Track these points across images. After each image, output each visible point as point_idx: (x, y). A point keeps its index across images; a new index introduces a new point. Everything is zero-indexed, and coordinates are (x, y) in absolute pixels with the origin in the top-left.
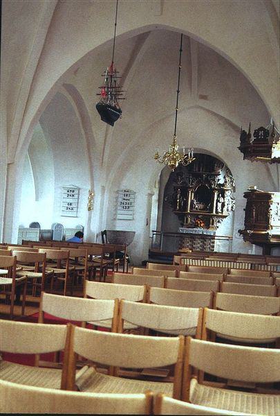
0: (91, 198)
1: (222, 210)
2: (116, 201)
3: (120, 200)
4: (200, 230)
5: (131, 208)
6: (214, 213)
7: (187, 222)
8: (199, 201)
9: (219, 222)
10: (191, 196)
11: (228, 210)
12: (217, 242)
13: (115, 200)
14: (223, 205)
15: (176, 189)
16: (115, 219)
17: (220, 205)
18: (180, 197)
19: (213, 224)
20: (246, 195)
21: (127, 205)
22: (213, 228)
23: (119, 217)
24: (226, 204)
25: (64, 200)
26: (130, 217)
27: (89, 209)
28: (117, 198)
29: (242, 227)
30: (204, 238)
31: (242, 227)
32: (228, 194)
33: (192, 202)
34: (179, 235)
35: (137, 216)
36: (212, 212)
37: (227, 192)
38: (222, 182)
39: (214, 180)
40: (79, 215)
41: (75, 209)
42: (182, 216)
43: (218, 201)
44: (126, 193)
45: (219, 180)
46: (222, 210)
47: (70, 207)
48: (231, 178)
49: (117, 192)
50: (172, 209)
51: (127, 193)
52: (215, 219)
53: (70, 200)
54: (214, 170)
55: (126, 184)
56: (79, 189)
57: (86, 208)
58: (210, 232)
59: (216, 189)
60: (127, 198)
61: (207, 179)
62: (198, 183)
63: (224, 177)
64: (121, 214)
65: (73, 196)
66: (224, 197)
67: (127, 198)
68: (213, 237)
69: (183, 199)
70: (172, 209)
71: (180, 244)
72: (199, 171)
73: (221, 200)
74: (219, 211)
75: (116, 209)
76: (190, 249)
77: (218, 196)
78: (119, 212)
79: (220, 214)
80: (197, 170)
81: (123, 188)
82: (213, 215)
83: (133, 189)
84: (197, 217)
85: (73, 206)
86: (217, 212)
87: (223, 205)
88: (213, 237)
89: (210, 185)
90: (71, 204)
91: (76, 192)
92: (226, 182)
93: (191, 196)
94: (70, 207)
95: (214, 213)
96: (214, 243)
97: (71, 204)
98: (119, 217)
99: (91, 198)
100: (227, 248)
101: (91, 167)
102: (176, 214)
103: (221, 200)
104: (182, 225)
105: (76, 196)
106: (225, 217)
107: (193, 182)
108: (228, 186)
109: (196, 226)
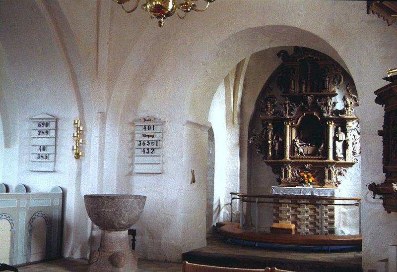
0: (80, 134)
1: (344, 154)
2: (133, 141)
3: (138, 137)
4: (308, 189)
5: (157, 152)
6: (331, 159)
7: (286, 177)
8: (305, 140)
9: (340, 174)
10: (291, 134)
11: (354, 153)
12: (338, 211)
13: (129, 138)
14: (345, 145)
15: (265, 125)
16: (130, 174)
17: (339, 145)
18: (272, 137)
19: (330, 178)
20: (377, 101)
21: (150, 146)
22: (330, 184)
23: (138, 168)
24: (350, 143)
25: (34, 142)
26: (156, 168)
27: (77, 156)
28: (133, 134)
29: (379, 178)
30: (314, 201)
31: (379, 178)
32: (352, 125)
33: (293, 143)
34: (272, 200)
35: (169, 166)
36: (327, 157)
37: (350, 123)
38: (340, 106)
39: (326, 105)
40: (60, 167)
41: (51, 157)
42: (278, 167)
43: (336, 139)
44: (147, 124)
45: (335, 104)
46: (344, 154)
47: (43, 154)
48: (355, 99)
49: (133, 124)
50: (262, 156)
51: (150, 124)
52: (334, 170)
53: (43, 141)
54: (324, 88)
55: (146, 108)
56: (57, 120)
57: (71, 155)
58: (325, 191)
59: (331, 119)
60: (150, 132)
61: (314, 103)
62: (302, 110)
63: (344, 99)
64: (143, 164)
65: (47, 132)
66: (345, 131)
67: (150, 132)
68: (330, 201)
69: (277, 139)
70: (262, 156)
71: (274, 215)
72: (301, 90)
73: (342, 136)
74: (340, 154)
75: (132, 156)
76: (293, 222)
77: (336, 131)
78: (137, 160)
79: (341, 161)
80: (297, 90)
81: (142, 115)
82: (332, 163)
83: (160, 115)
84: (300, 166)
85: (50, 150)
86: (335, 157)
87: (345, 145)
88: (330, 201)
89: (321, 113)
90: (44, 149)
91: (52, 125)
92: (347, 106)
93: (291, 134)
94: (43, 154)
95: (331, 159)
96: (332, 210)
97: (44, 149)
98: (138, 168)
99: (80, 134)
100: (170, 260)
101: (74, 77)
102: (268, 163)
103: (342, 136)
104: (279, 182)
105: (52, 133)
106: (350, 165)
107: (291, 110)
108: (350, 113)
109: (301, 182)
